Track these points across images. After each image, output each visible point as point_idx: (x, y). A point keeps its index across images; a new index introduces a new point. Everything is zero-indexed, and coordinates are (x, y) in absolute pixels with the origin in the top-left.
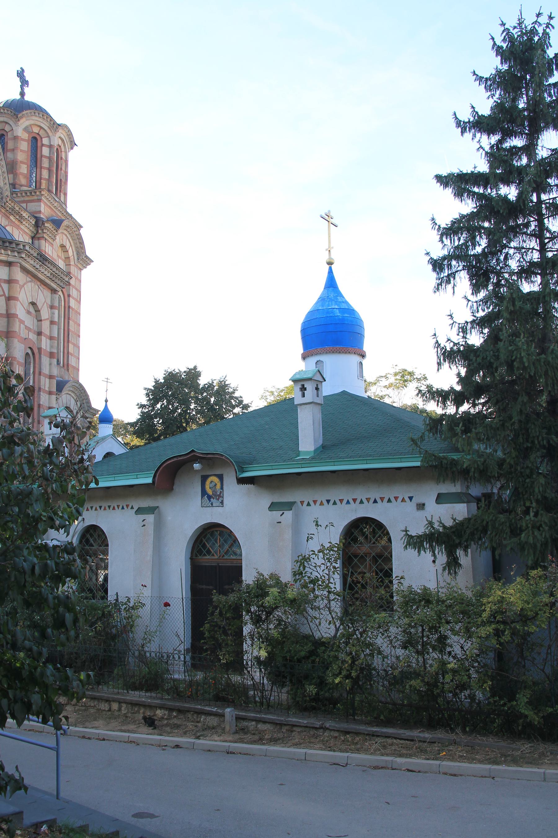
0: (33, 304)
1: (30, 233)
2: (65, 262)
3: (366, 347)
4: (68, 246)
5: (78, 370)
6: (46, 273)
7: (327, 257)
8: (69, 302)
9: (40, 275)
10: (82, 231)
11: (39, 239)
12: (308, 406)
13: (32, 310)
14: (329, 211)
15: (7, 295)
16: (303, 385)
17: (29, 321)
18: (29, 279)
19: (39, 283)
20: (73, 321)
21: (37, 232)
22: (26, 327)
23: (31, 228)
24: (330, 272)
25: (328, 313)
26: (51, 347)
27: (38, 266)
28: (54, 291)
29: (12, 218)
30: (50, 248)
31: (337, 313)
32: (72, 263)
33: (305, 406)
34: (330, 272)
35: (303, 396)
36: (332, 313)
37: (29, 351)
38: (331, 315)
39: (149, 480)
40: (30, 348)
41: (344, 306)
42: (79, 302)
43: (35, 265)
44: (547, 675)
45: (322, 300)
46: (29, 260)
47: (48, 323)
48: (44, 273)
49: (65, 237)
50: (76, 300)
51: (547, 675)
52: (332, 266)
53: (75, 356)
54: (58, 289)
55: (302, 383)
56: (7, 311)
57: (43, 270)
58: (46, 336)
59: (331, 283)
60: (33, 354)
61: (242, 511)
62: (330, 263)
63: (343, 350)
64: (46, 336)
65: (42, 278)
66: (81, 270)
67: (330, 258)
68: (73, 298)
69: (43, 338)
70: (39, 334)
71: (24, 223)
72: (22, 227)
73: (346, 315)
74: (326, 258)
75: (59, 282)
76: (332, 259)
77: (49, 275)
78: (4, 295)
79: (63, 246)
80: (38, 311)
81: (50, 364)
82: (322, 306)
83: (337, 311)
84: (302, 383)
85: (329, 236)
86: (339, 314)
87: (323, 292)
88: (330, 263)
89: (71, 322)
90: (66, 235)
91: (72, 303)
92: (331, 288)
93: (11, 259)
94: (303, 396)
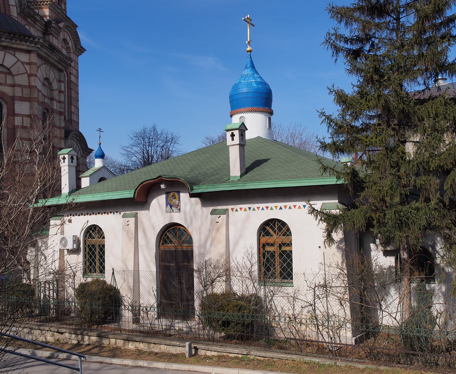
0: (47, 79)
1: (42, 31)
2: (66, 50)
4: (68, 39)
5: (78, 123)
6: (55, 58)
8: (70, 78)
9: (50, 59)
13: (46, 83)
15: (29, 73)
16: (233, 133)
17: (44, 91)
18: (43, 62)
20: (74, 90)
21: (47, 31)
22: (43, 95)
26: (60, 108)
27: (49, 54)
28: (60, 71)
29: (29, 20)
30: (56, 41)
32: (72, 51)
37: (45, 111)
39: (131, 196)
40: (46, 108)
42: (77, 78)
47: (57, 92)
48: (54, 58)
49: (66, 33)
53: (76, 114)
56: (29, 83)
57: (53, 56)
58: (56, 100)
61: (190, 212)
64: (56, 100)
65: (53, 61)
68: (73, 75)
69: (55, 102)
70: (52, 99)
71: (38, 23)
72: (36, 26)
75: (64, 65)
77: (57, 59)
78: (27, 73)
79: (65, 40)
80: (50, 84)
81: (60, 120)
89: (72, 91)
90: (67, 32)
91: (73, 78)
93: (30, 48)
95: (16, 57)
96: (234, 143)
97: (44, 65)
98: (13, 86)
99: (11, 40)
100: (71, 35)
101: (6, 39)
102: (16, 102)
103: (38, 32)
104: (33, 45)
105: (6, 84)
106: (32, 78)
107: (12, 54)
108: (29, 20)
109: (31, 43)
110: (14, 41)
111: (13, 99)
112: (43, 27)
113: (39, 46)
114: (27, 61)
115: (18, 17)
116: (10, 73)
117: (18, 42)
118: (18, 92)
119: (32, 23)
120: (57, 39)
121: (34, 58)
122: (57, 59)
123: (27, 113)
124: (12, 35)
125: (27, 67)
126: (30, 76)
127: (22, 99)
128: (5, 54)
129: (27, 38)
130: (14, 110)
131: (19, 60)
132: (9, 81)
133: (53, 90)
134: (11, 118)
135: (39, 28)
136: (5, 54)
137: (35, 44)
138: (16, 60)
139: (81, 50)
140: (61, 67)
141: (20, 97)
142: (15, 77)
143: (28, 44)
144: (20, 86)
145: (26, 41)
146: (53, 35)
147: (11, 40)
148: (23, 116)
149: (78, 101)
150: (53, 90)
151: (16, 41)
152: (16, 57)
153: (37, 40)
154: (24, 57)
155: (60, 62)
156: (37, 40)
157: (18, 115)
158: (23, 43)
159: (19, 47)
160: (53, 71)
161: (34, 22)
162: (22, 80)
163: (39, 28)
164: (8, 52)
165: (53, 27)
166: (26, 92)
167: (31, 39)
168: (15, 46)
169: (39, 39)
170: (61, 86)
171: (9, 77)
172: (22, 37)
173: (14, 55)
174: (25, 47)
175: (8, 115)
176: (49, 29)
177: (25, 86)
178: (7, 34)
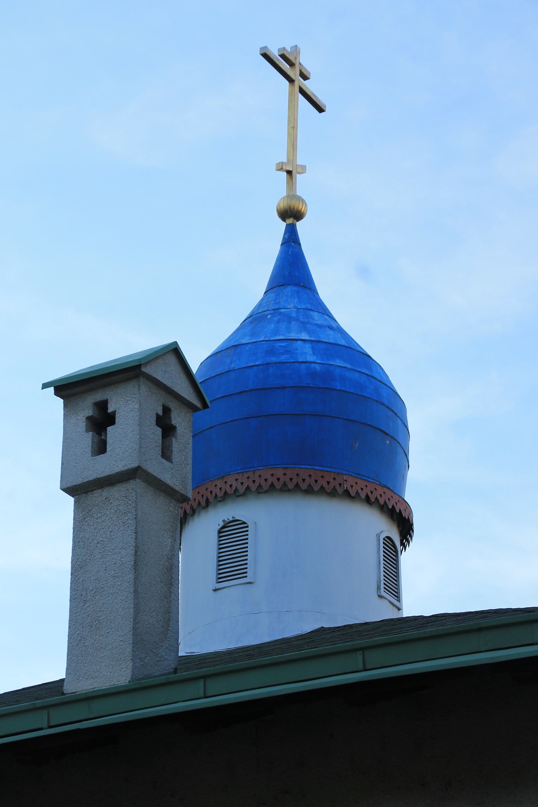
3: (417, 489)
7: (283, 192)
12: (116, 492)
14: (296, 48)
16: (102, 406)
24: (291, 239)
25: (271, 352)
31: (307, 354)
33: (106, 492)
34: (291, 239)
35: (101, 448)
36: (287, 352)
38: (283, 358)
41: (330, 337)
45: (255, 319)
52: (299, 225)
55: (99, 396)
59: (292, 272)
62: (291, 214)
63: (322, 482)
67: (292, 194)
73: (339, 362)
74: (277, 192)
76: (300, 199)
82: (253, 335)
83: (308, 348)
84: (99, 396)
86: (311, 358)
87: (262, 300)
88: (291, 214)
92: (289, 289)
94: (101, 448)
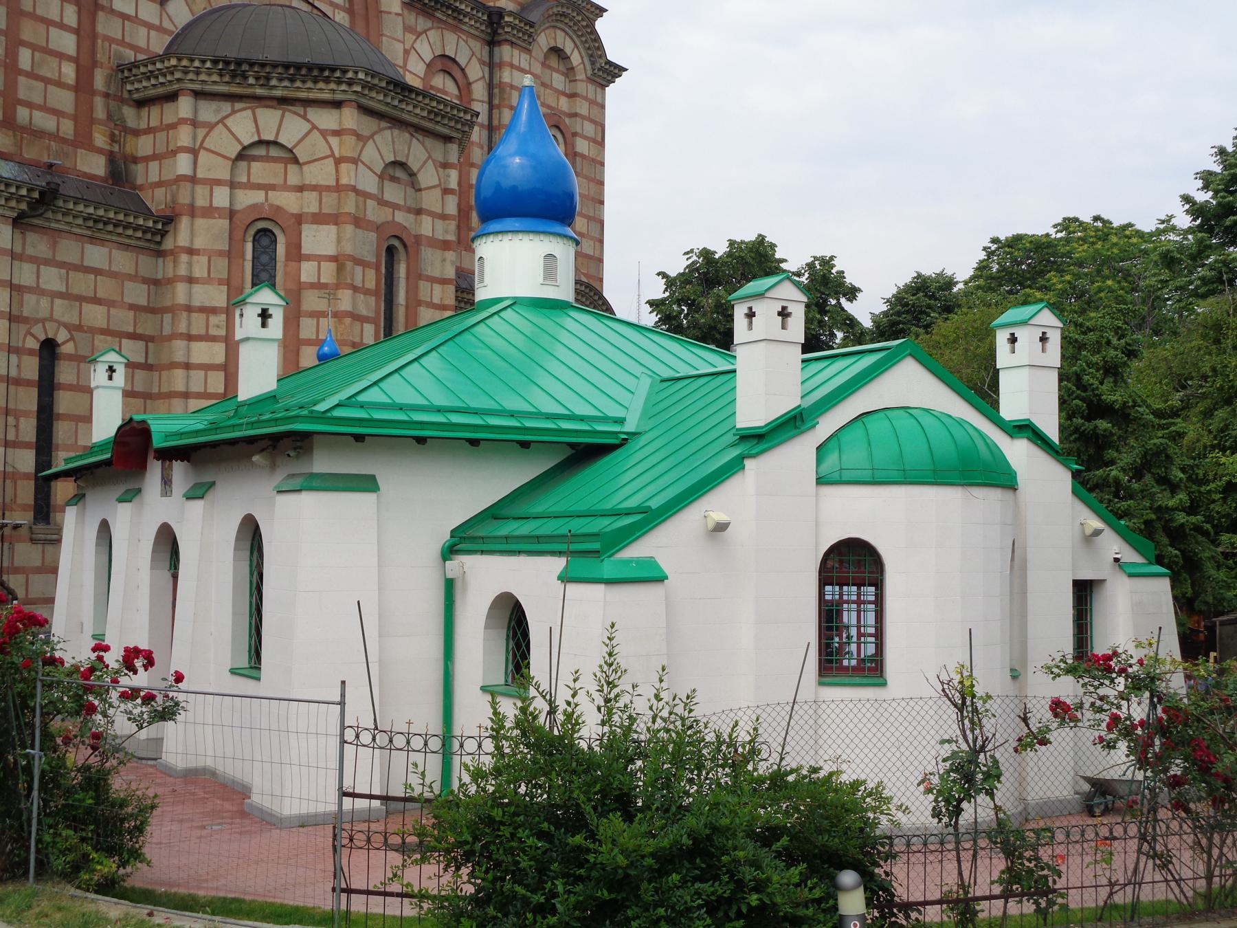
4: (568, 47)
6: (418, 111)
9: (406, 117)
10: (601, 25)
11: (500, 43)
15: (337, 155)
18: (384, 124)
19: (411, 130)
23: (483, 28)
27: (396, 103)
29: (438, 15)
30: (525, 56)
37: (396, 243)
39: (109, 456)
43: (389, 100)
44: (447, 738)
46: (374, 94)
47: (437, 193)
48: (413, 112)
49: (559, 33)
50: (594, 141)
51: (447, 738)
53: (592, 238)
54: (454, 134)
55: (785, 304)
56: (337, 180)
57: (410, 108)
60: (405, 246)
66: (603, 87)
71: (467, 20)
75: (452, 124)
77: (425, 114)
78: (333, 155)
79: (557, 51)
80: (412, 175)
84: (749, 305)
85: (233, 134)
90: (563, 30)
91: (582, 146)
93: (339, 97)
95: (308, 121)
96: (264, 333)
97: (388, 133)
98: (301, 189)
99: (292, 80)
100: (578, 36)
101: (281, 80)
102: (305, 227)
103: (472, 42)
104: (344, 87)
105: (285, 187)
106: (344, 167)
107: (299, 115)
108: (438, 15)
109: (339, 82)
110: (298, 84)
111: (299, 219)
112: (483, 28)
113: (359, 89)
114: (335, 127)
115: (406, 12)
116: (295, 161)
117: (309, 84)
118: (310, 202)
119: (450, 21)
120: (529, 51)
121: (349, 118)
122: (425, 114)
123: (331, 251)
124: (292, 71)
125: (334, 141)
126: (338, 161)
127: (319, 219)
128: (283, 116)
129: (327, 73)
130: (299, 246)
131: (314, 127)
132: (293, 180)
133: (420, 190)
134: (293, 264)
135: (472, 31)
136: (283, 116)
137: (350, 84)
138: (309, 126)
139: (613, 72)
140: (446, 131)
141: (314, 214)
142: (305, 168)
143: (333, 86)
144: (315, 188)
145: (327, 80)
146: (512, 44)
147: (292, 80)
148: (319, 259)
149: (602, 203)
150: (420, 190)
151: (304, 82)
152: (308, 121)
153: (350, 75)
154: (326, 119)
155: (439, 119)
156: (350, 75)
157: (309, 258)
158: (321, 85)
159: (312, 96)
160: (423, 144)
161: (455, 18)
162: (322, 173)
163: (472, 31)
164: (290, 111)
165: (508, 24)
166: (330, 203)
167: (338, 74)
168: (303, 95)
169: (356, 73)
170: (449, 176)
171: (292, 168)
172: (315, 73)
173: (304, 117)
174: (326, 96)
175: (288, 257)
176: (500, 31)
177: (328, 188)
178: (280, 70)
